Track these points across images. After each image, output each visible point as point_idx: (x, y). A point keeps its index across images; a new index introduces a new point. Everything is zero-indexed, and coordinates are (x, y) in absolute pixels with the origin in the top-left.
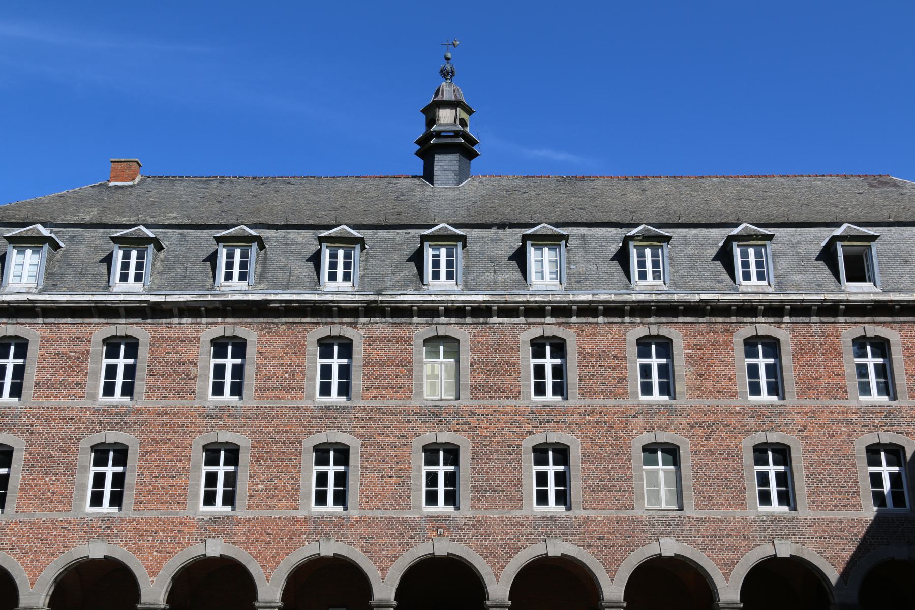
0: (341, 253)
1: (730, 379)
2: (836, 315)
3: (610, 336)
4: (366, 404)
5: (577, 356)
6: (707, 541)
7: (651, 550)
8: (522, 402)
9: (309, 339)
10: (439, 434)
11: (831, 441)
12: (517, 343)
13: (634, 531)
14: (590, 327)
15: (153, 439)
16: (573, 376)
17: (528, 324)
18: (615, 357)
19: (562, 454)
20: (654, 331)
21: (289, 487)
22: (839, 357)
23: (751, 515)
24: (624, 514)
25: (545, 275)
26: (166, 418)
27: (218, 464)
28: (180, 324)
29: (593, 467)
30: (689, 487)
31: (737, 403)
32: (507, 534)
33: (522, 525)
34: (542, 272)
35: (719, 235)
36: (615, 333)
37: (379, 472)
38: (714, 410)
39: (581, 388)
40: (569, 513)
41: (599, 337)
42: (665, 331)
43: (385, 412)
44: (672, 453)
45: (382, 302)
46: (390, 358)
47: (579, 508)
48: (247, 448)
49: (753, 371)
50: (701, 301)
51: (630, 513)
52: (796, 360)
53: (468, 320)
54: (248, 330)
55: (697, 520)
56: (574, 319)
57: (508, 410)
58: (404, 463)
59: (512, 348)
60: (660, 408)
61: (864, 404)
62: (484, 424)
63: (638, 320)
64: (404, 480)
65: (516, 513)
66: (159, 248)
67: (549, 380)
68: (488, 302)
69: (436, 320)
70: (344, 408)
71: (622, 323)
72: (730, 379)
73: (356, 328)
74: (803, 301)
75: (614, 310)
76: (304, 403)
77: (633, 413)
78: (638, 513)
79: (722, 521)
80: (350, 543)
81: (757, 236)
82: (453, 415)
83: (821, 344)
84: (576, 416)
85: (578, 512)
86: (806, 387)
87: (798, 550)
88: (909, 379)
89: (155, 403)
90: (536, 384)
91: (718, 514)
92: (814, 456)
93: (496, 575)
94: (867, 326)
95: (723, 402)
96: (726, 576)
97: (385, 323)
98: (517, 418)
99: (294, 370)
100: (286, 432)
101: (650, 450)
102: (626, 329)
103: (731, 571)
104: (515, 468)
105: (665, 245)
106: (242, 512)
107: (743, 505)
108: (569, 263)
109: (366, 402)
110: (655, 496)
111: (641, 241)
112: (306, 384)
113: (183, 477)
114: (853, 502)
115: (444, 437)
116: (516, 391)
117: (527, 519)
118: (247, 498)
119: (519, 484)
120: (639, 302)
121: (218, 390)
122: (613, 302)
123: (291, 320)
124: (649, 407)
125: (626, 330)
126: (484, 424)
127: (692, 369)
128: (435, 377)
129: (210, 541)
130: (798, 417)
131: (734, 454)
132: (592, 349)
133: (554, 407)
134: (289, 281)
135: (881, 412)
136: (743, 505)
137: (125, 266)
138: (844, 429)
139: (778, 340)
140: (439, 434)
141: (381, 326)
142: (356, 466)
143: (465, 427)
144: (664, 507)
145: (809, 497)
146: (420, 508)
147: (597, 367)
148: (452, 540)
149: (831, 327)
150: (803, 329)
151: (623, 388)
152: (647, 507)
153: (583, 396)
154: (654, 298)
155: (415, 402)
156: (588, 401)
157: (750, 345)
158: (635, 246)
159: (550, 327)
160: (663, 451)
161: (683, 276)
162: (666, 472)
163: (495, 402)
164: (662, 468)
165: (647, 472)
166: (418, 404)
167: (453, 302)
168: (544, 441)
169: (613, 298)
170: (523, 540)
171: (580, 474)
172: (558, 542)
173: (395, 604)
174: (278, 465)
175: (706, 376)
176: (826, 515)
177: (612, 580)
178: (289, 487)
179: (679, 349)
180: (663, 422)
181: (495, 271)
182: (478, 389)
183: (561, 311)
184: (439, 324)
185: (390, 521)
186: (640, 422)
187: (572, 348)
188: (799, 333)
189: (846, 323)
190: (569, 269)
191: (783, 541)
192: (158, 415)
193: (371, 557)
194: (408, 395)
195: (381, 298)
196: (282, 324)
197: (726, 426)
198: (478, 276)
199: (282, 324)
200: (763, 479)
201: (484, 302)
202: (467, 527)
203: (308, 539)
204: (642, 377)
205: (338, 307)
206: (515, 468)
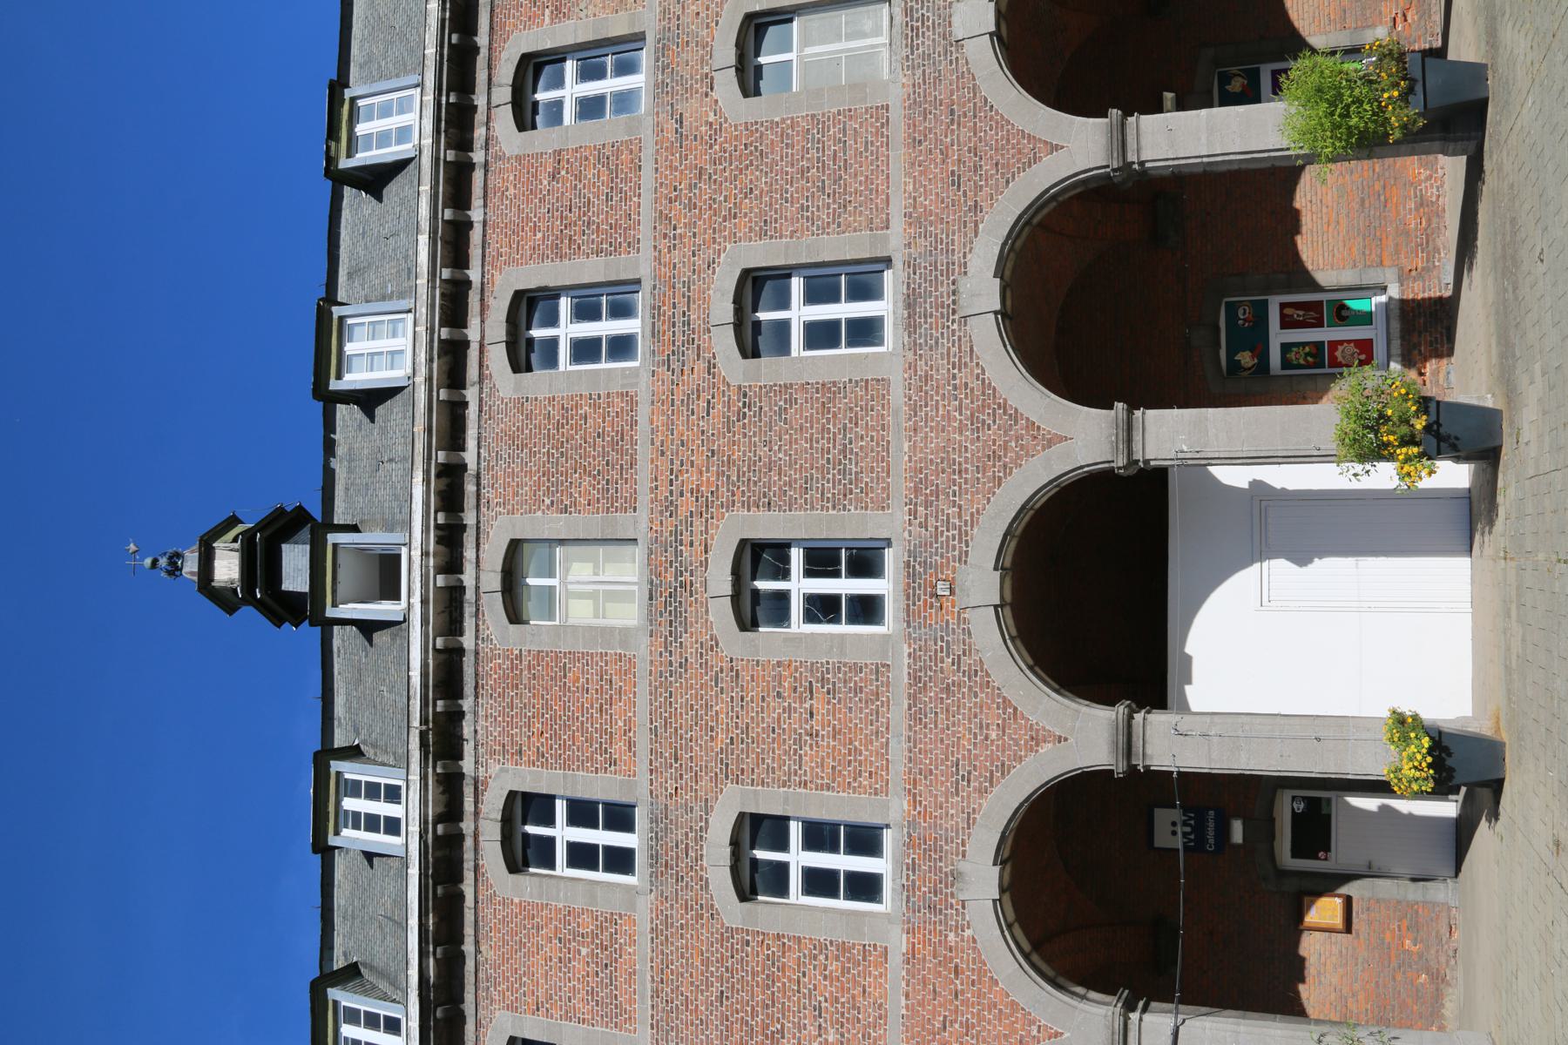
0: (349, 804)
3: (512, 191)
4: (645, 766)
5: (548, 263)
7: (983, 59)
10: (712, 591)
12: (520, 403)
13: (936, 101)
16: (590, 269)
17: (481, 381)
19: (757, 286)
21: (834, 966)
24: (898, 129)
25: (385, 346)
29: (791, 210)
32: (948, 417)
33: (927, 378)
34: (393, 353)
37: (799, 742)
39: (616, 249)
40: (898, 263)
41: (512, 215)
43: (663, 724)
44: (756, 27)
45: (424, 721)
51: (897, 115)
53: (469, 518)
56: (474, 274)
57: (660, 420)
58: (779, 679)
62: (690, 478)
63: (479, 133)
64: (821, 680)
65: (897, 396)
68: (427, 472)
69: (470, 595)
70: (654, 820)
73: (485, 783)
75: (456, 184)
78: (896, 97)
84: (676, 256)
85: (895, 241)
93: (1050, 443)
97: (476, 713)
99: (575, 934)
100: (706, 963)
101: (749, 79)
102: (498, 158)
104: (791, 401)
106: (890, 812)
108: (383, 298)
109: (642, 767)
111: (338, 140)
112: (602, 908)
116: (619, 404)
117: (912, 366)
119: (829, 390)
120: (437, 130)
123: (469, 930)
125: (500, 157)
126: (690, 478)
128: (595, 592)
129: (959, 33)
132: (535, 229)
140: (712, 591)
141: (482, 722)
142: (786, 800)
143: (698, 524)
146: (885, 638)
147: (573, 217)
148: (963, 558)
151: (618, 153)
153: (634, 244)
155: (642, 649)
156: (645, 232)
159: (487, 328)
162: (805, 42)
163: (644, 452)
166: (646, 640)
167: (425, 554)
168: (730, 330)
170: (962, 376)
171: (808, 239)
172: (965, 285)
174: (783, 989)
177: (1057, 148)
178: (834, 966)
180: (691, 55)
181: (391, 460)
182: (615, 498)
183: (454, 304)
184: (477, 588)
186: (691, 108)
190: (391, 297)
193: (1004, 770)
194: (627, 664)
195: (416, 723)
196: (478, 951)
199: (478, 951)
201: (427, 481)
202: (931, 521)
203: (960, 929)
206: (791, 401)
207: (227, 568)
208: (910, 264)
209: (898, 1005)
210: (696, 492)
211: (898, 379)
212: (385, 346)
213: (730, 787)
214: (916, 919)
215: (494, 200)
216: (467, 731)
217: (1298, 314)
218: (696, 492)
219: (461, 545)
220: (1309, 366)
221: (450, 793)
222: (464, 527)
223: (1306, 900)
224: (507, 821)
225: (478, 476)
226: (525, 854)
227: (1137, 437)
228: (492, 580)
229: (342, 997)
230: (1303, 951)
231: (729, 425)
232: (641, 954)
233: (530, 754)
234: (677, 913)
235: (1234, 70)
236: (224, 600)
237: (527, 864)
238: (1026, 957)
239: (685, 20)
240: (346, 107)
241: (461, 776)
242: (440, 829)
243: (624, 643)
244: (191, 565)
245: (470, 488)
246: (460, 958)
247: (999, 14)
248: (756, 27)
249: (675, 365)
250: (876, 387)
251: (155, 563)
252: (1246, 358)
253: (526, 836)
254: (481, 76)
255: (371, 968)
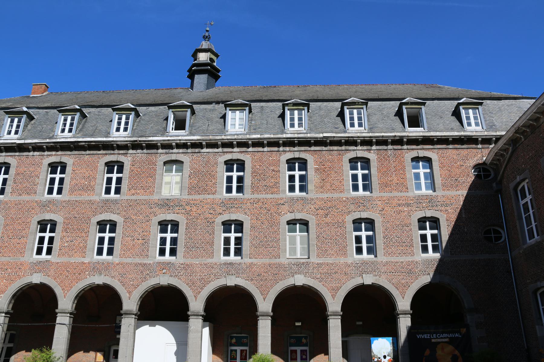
0: (124, 117)
1: (340, 182)
2: (402, 145)
3: (271, 159)
5: (251, 169)
6: (323, 276)
8: (217, 196)
9: (100, 163)
11: (398, 217)
12: (216, 163)
13: (279, 270)
14: (259, 154)
15: (12, 218)
16: (247, 182)
18: (273, 170)
20: (297, 155)
21: (82, 245)
22: (403, 168)
23: (349, 261)
24: (274, 261)
26: (20, 206)
27: (230, 232)
28: (33, 155)
29: (257, 234)
30: (313, 245)
31: (344, 196)
33: (213, 268)
35: (455, 103)
36: (274, 156)
38: (330, 200)
39: (252, 188)
41: (265, 159)
42: (303, 155)
45: (140, 141)
46: (143, 172)
47: (247, 258)
48: (61, 223)
49: (355, 178)
50: (324, 137)
51: (277, 261)
52: (379, 170)
53: (190, 150)
54: (68, 158)
55: (318, 264)
56: (251, 149)
59: (213, 166)
60: (298, 199)
61: (417, 195)
62: (194, 209)
63: (287, 149)
64: (146, 241)
65: (209, 260)
66: (137, 115)
67: (297, 184)
68: (200, 140)
69: (171, 151)
71: (278, 151)
72: (340, 182)
73: (126, 156)
74: (383, 137)
76: (95, 198)
77: (282, 202)
78: (282, 260)
79: (332, 264)
80: (112, 277)
81: (359, 103)
82: (177, 204)
83: (394, 161)
84: (249, 204)
86: (384, 186)
87: (376, 280)
88: (442, 180)
89: (15, 198)
90: (353, 185)
91: (330, 260)
92: (388, 225)
93: (195, 297)
94: (419, 151)
95: (336, 195)
96: (333, 296)
98: (214, 206)
100: (83, 214)
101: (291, 223)
103: (336, 293)
104: (210, 234)
105: (479, 107)
107: (345, 255)
110: (293, 250)
111: (293, 106)
112: (96, 187)
113: (25, 239)
114: (409, 251)
115: (169, 217)
116: (214, 190)
118: (58, 251)
119: (212, 244)
120: (287, 138)
121: (229, 190)
122: (272, 138)
123: (92, 152)
124: (292, 199)
125: (280, 155)
127: (318, 176)
128: (171, 184)
129: (296, 276)
130: (379, 203)
131: (341, 225)
132: (260, 166)
133: (235, 199)
134: (94, 132)
135: (427, 199)
136: (345, 255)
137: (119, 124)
138: (405, 209)
139: (369, 159)
141: (141, 155)
142: (119, 233)
143: (183, 211)
144: (299, 256)
145: (384, 249)
147: (262, 176)
148: (171, 276)
149: (399, 152)
150: (383, 153)
151: (277, 188)
152: (288, 256)
153: (253, 193)
154: (296, 136)
155: (155, 197)
156: (256, 196)
157: (353, 162)
158: (463, 108)
160: (299, 224)
161: (316, 126)
162: (301, 236)
163: (201, 197)
164: (299, 235)
165: (290, 236)
167: (180, 140)
169: (272, 136)
170: (212, 276)
171: (249, 238)
172: (233, 277)
173: (272, 314)
175: (326, 180)
176: (394, 259)
177: (264, 300)
178: (82, 245)
179: (311, 165)
180: (300, 207)
183: (242, 144)
185: (136, 265)
186: (286, 207)
187: (248, 166)
188: (381, 155)
189: (408, 149)
191: (368, 275)
192: (16, 204)
193: (123, 285)
194: (152, 193)
195: (140, 139)
196: (87, 155)
197: (337, 209)
198: (198, 128)
199: (87, 155)
200: (358, 240)
201: (198, 140)
204: (353, 181)
205: (4, 147)
206: (210, 234)
207: (203, 57)
208: (240, 264)
209: (72, 260)
210: (191, 210)
211: (214, 260)
212: (237, 124)
213: (123, 219)
214: (92, 265)
215: (269, 154)
216: (139, 151)
217: (244, 354)
218: (191, 210)
219: (183, 148)
220: (231, 356)
221: (123, 147)
222: (187, 149)
223: (102, 353)
224: (117, 162)
225: (200, 152)
226: (110, 167)
227: (195, 317)
228: (174, 157)
229: (77, 116)
230: (91, 352)
231: (206, 219)
232: (86, 197)
233: (132, 169)
234: (95, 206)
235: (308, 340)
236: (195, 56)
237: (108, 166)
238: (83, 290)
239: (310, 205)
240: (302, 108)
241: (128, 150)
242: (115, 145)
243: (157, 192)
244: (205, 45)
245: (197, 150)
246: (85, 150)
247: (302, 286)
248: (305, 224)
249: (222, 205)
250: (211, 255)
251: (207, 31)
252: (234, 341)
253: (114, 166)
254: (303, 148)
255: (85, 122)
